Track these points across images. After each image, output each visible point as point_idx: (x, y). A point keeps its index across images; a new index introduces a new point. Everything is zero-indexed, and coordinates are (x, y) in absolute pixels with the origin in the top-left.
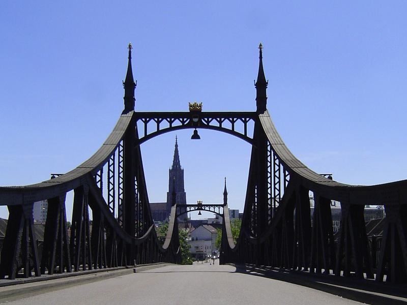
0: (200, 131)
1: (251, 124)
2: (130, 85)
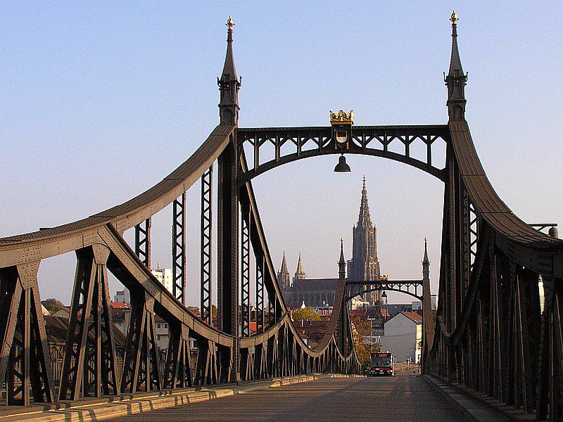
0: (350, 158)
1: (440, 146)
2: (229, 84)
